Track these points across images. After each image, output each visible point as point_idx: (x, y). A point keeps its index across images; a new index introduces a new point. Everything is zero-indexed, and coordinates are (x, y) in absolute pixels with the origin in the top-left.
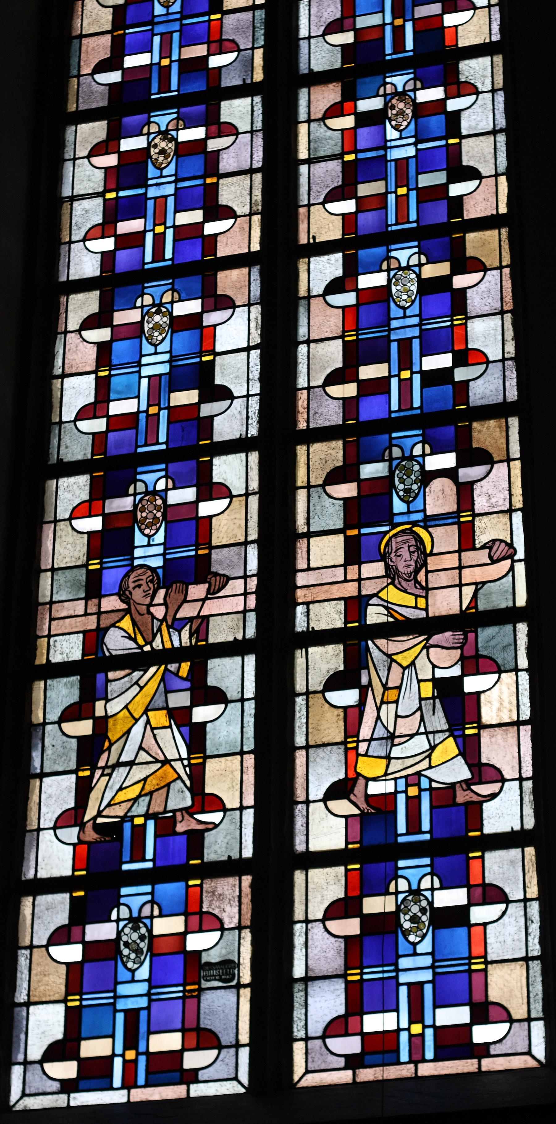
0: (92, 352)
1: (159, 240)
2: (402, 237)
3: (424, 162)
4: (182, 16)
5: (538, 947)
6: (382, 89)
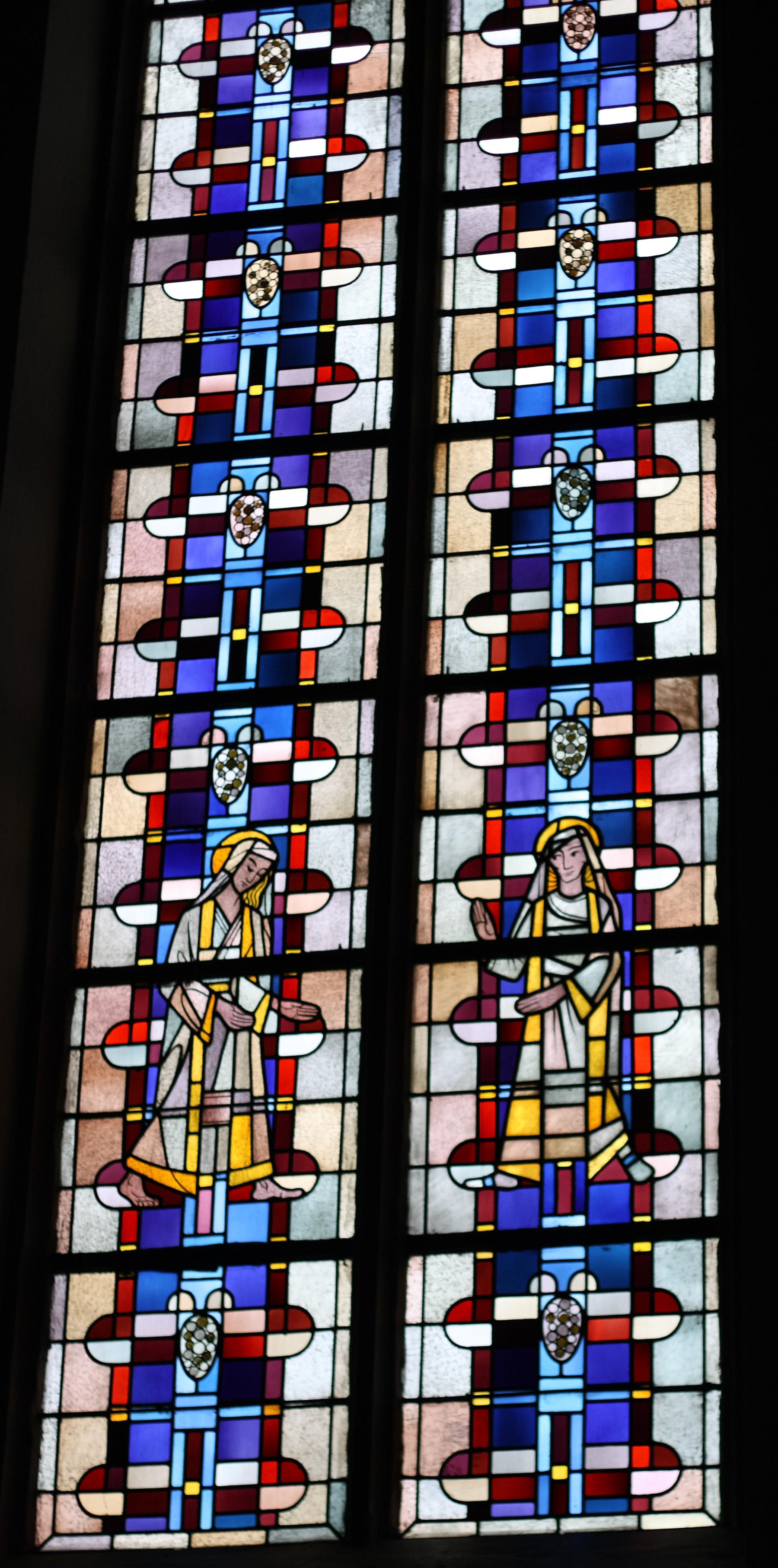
0: (129, 938)
1: (238, 650)
2: (576, 189)
3: (598, 832)
4: (292, 97)
5: (712, 277)
6: (549, 456)
